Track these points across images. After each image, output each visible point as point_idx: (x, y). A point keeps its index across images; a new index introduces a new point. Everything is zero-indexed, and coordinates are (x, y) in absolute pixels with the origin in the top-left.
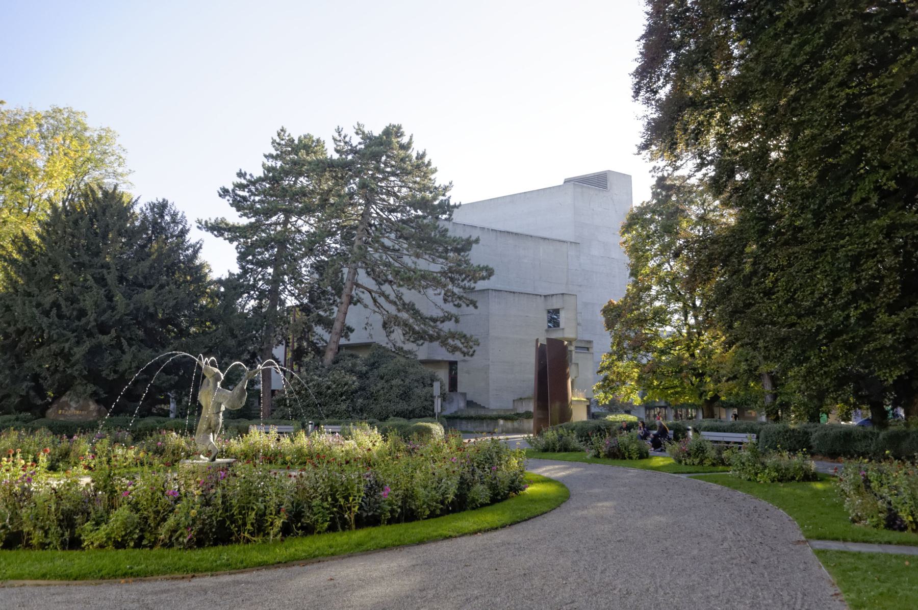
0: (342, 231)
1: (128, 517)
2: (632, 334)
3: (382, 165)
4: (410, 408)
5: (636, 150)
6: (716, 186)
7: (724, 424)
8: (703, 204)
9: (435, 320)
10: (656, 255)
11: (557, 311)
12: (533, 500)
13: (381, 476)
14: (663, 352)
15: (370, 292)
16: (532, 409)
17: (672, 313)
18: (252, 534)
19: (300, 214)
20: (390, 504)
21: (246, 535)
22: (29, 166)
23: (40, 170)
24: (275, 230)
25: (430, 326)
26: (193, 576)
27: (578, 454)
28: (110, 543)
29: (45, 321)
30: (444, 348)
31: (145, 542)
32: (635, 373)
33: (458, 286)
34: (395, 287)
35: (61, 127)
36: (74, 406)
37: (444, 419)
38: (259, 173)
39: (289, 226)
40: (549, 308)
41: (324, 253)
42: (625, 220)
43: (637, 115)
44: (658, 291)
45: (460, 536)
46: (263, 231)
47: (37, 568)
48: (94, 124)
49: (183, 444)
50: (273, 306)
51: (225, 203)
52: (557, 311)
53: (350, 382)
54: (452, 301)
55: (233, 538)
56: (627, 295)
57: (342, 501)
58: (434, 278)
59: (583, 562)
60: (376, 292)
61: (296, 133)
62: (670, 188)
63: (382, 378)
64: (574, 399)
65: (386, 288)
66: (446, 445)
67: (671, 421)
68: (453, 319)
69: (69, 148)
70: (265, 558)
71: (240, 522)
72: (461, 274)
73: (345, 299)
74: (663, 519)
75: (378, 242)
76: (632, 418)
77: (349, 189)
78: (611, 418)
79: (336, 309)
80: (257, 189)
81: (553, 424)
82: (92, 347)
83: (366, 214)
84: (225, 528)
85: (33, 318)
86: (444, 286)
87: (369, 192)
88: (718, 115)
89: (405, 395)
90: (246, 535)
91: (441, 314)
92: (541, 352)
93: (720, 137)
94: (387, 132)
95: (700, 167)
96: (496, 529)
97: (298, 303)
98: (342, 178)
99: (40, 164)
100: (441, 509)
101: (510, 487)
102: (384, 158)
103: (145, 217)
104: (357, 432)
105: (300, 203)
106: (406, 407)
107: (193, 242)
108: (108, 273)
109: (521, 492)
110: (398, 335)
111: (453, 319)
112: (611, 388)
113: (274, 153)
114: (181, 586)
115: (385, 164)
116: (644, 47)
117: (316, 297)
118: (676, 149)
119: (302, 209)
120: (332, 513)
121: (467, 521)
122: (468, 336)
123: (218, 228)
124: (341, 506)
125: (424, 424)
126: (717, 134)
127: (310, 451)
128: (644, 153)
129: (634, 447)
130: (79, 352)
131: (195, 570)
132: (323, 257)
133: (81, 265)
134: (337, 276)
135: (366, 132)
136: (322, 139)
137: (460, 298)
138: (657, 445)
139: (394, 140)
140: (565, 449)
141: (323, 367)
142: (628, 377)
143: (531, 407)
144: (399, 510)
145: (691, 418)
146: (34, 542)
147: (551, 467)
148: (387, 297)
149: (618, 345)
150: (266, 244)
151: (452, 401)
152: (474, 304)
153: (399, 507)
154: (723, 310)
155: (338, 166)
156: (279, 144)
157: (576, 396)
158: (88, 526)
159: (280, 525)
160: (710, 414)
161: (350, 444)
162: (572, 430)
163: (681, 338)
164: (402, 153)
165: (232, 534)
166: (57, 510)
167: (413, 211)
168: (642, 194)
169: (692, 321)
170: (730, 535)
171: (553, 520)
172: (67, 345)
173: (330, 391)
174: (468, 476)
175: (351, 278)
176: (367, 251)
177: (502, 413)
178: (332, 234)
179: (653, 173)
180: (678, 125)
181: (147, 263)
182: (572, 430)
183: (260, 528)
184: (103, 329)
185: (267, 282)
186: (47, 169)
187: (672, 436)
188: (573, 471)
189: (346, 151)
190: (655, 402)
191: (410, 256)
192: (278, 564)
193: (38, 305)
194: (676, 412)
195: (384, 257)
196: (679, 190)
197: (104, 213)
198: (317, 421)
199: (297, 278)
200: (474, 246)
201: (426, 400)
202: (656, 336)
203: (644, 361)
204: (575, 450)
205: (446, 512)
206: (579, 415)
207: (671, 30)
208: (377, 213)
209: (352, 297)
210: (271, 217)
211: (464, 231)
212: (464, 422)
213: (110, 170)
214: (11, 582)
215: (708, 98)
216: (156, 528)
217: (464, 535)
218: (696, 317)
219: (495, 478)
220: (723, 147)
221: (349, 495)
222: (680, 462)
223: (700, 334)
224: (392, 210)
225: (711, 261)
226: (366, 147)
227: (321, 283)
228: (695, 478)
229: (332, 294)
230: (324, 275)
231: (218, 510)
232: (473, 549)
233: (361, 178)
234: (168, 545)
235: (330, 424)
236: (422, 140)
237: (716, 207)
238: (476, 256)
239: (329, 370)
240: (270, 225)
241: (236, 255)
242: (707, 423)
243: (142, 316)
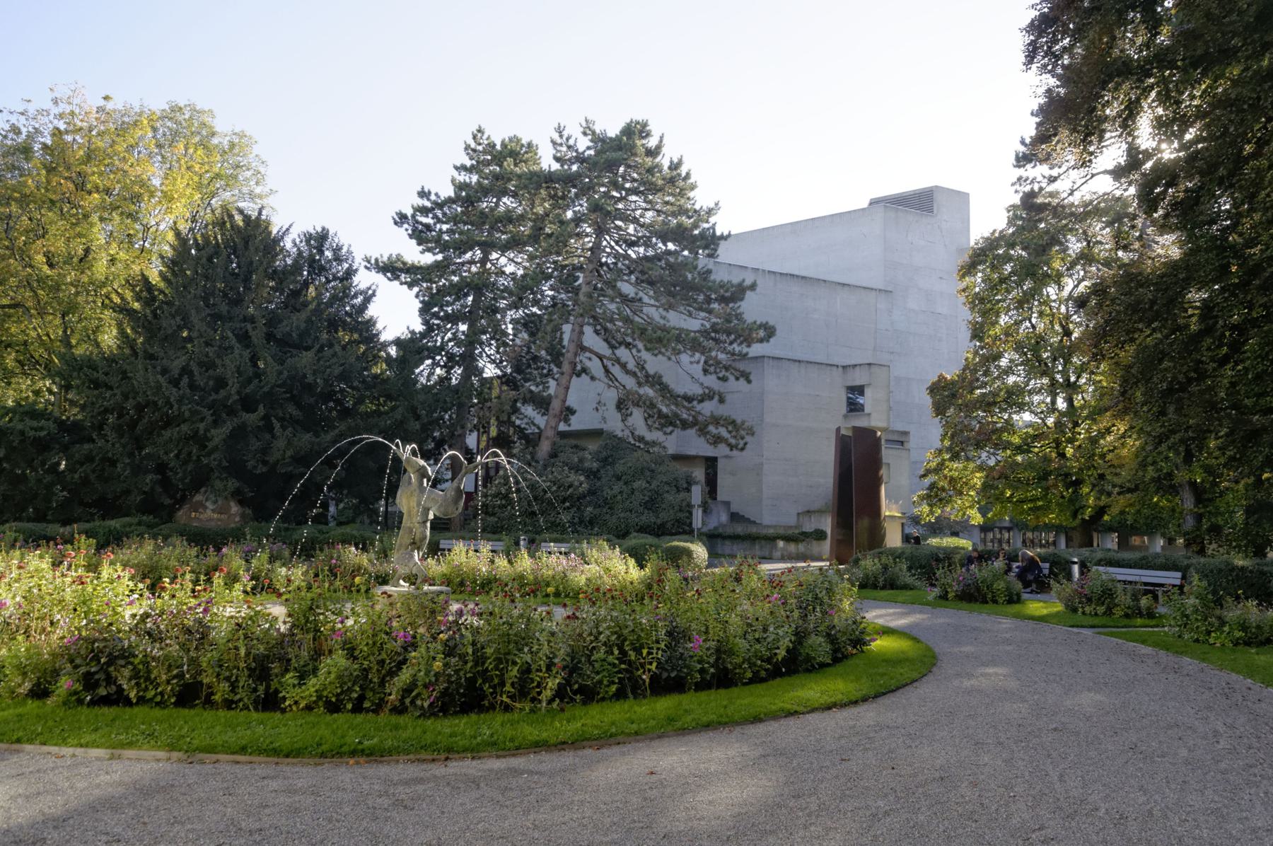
1: (346, 669)
4: (659, 522)
9: (689, 399)
11: (860, 390)
14: (1019, 449)
15: (601, 358)
18: (512, 697)
19: (504, 248)
20: (699, 662)
21: (505, 698)
22: (143, 184)
23: (156, 190)
24: (469, 271)
26: (447, 759)
28: (321, 703)
29: (174, 393)
30: (702, 439)
31: (367, 704)
32: (978, 479)
33: (724, 351)
34: (634, 351)
35: (182, 131)
36: (211, 507)
37: (705, 538)
38: (448, 191)
39: (489, 265)
41: (536, 303)
46: (454, 273)
47: (231, 737)
48: (224, 125)
49: (365, 562)
50: (466, 377)
51: (402, 233)
52: (860, 390)
53: (576, 483)
55: (486, 703)
57: (632, 655)
60: (609, 359)
61: (498, 136)
63: (619, 478)
65: (623, 353)
68: (717, 398)
69: (191, 158)
70: (545, 735)
71: (496, 681)
72: (729, 334)
73: (566, 367)
78: (934, 541)
79: (552, 383)
80: (444, 214)
82: (234, 428)
83: (596, 249)
84: (476, 690)
85: (159, 387)
87: (602, 216)
89: (652, 504)
90: (505, 698)
97: (499, 373)
98: (563, 197)
99: (156, 182)
102: (622, 169)
103: (300, 253)
105: (503, 233)
107: (362, 286)
108: (254, 329)
110: (637, 418)
111: (717, 398)
113: (468, 163)
114: (437, 773)
117: (522, 368)
119: (508, 242)
121: (812, 690)
122: (739, 421)
123: (392, 269)
125: (682, 544)
127: (536, 578)
130: (219, 435)
131: (449, 750)
132: (535, 310)
133: (217, 317)
135: (598, 131)
136: (534, 143)
139: (639, 143)
140: (892, 584)
143: (827, 524)
146: (217, 697)
147: (883, 611)
148: (623, 366)
150: (459, 291)
152: (746, 376)
156: (474, 150)
157: (889, 509)
158: (290, 678)
159: (555, 687)
165: (483, 697)
166: (248, 654)
167: (660, 245)
168: (989, 216)
172: (202, 426)
177: (781, 532)
179: (1017, 187)
181: (303, 315)
183: (525, 690)
184: (248, 404)
185: (459, 343)
186: (164, 188)
189: (570, 160)
192: (562, 745)
193: (165, 371)
197: (246, 248)
198: (531, 535)
199: (498, 335)
202: (1009, 424)
203: (992, 462)
204: (906, 587)
206: (893, 539)
208: (612, 248)
210: (465, 253)
212: (727, 542)
213: (245, 190)
214: (201, 756)
216: (382, 683)
217: (813, 710)
221: (642, 647)
222: (1075, 610)
224: (632, 244)
226: (598, 153)
228: (1112, 635)
229: (546, 361)
231: (466, 663)
232: (822, 727)
234: (399, 710)
236: (676, 142)
238: (752, 309)
240: (463, 264)
241: (417, 305)
243: (297, 388)
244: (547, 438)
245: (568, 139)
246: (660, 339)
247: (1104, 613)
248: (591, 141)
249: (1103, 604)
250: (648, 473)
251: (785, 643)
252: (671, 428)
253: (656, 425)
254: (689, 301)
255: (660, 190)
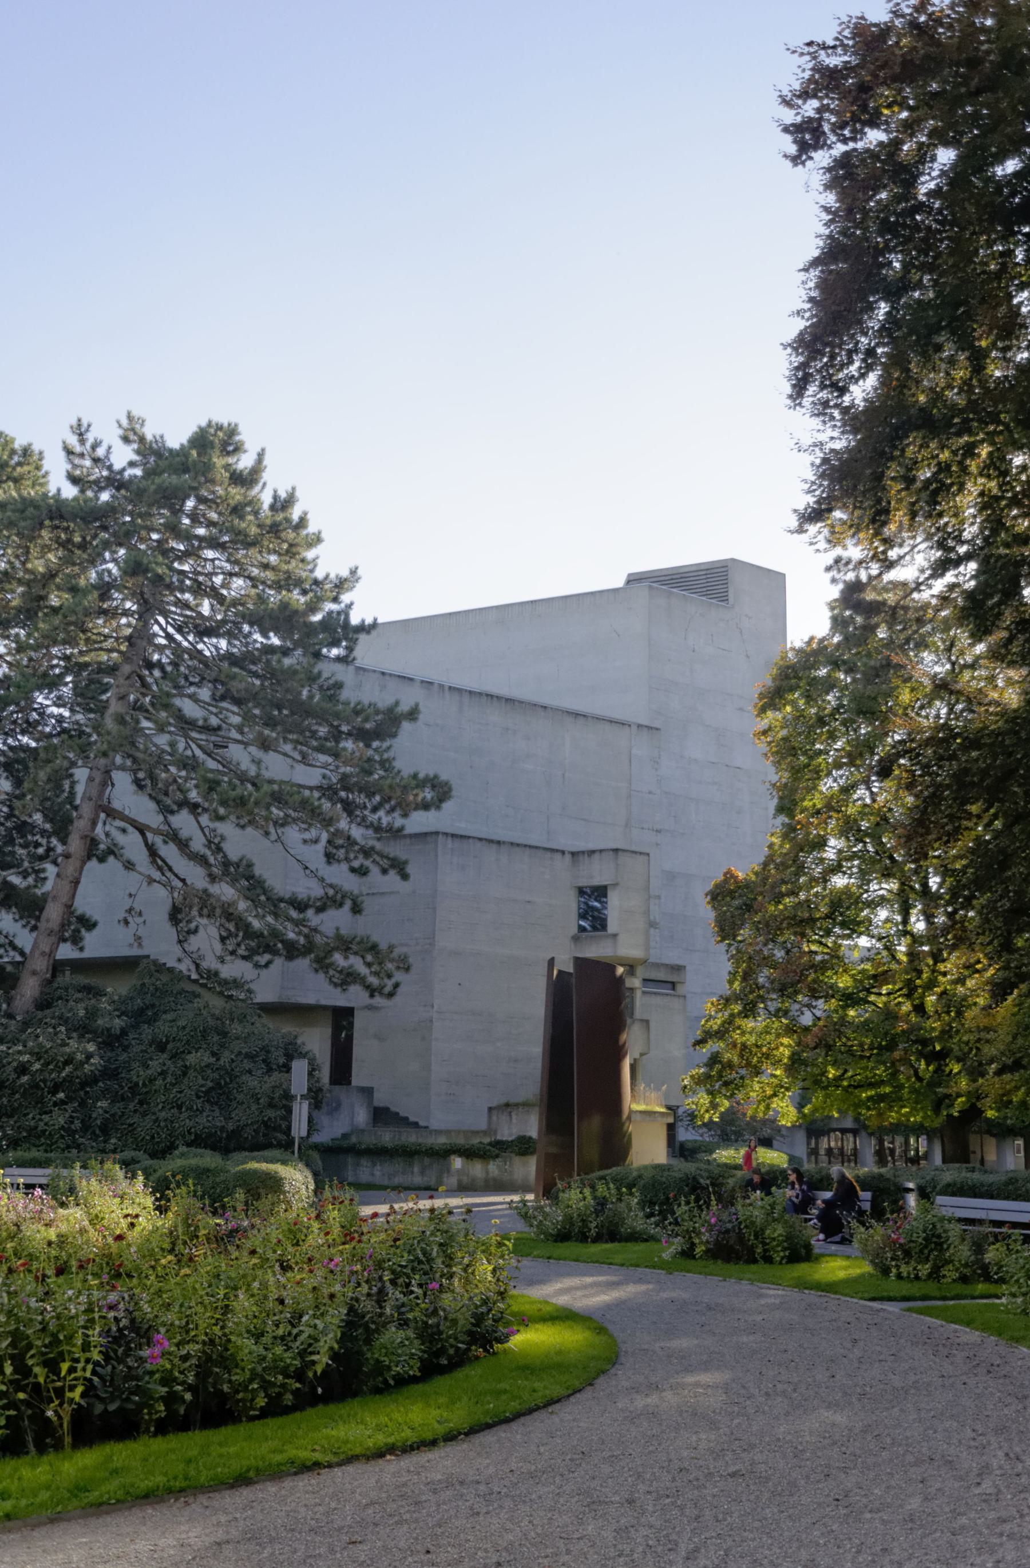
0: (77, 675)
2: (779, 954)
3: (186, 521)
4: (231, 1126)
5: (794, 522)
6: (977, 612)
7: (990, 1178)
8: (949, 649)
9: (301, 906)
10: (838, 766)
11: (601, 892)
12: (531, 1367)
13: (146, 1308)
14: (850, 999)
15: (142, 830)
16: (533, 1132)
17: (874, 904)
25: (289, 919)
27: (641, 1247)
30: (321, 975)
33: (363, 822)
34: (204, 819)
37: (315, 1156)
40: (583, 882)
42: (767, 679)
43: (792, 444)
44: (840, 852)
45: (340, 1464)
52: (601, 892)
53: (79, 1057)
54: (347, 859)
56: (769, 860)
58: (304, 803)
59: (644, 1531)
60: (157, 832)
62: (873, 609)
63: (162, 1048)
64: (636, 1107)
65: (183, 821)
66: (316, 1225)
67: (869, 1167)
72: (370, 795)
73: (76, 844)
74: (839, 1418)
75: (167, 706)
76: (771, 1157)
77: (100, 575)
79: (51, 870)
81: (586, 1169)
83: (140, 638)
86: (328, 822)
87: (150, 585)
88: (984, 451)
89: (220, 1094)
91: (316, 891)
92: (560, 990)
93: (987, 502)
94: (202, 440)
95: (940, 568)
96: (433, 1443)
98: (83, 546)
100: (296, 1393)
101: (470, 1333)
102: (190, 504)
104: (89, 1185)
106: (220, 1122)
109: (497, 1347)
110: (207, 939)
111: (348, 904)
112: (726, 1084)
115: (194, 517)
116: (817, 286)
118: (885, 523)
120: (13, 1405)
121: (361, 1424)
122: (383, 946)
124: (37, 1386)
125: (264, 1166)
126: (982, 494)
128: (813, 529)
129: (778, 1231)
132: (25, 740)
134: (59, 787)
135: (149, 437)
136: (36, 448)
137: (367, 852)
138: (832, 1227)
139: (218, 461)
140: (612, 1233)
141: (10, 1016)
142: (767, 1056)
143: (531, 1126)
144: (188, 1396)
145: (915, 1160)
147: (575, 1281)
148: (183, 845)
149: (746, 977)
151: (338, 1107)
152: (400, 868)
153: (189, 1388)
154: (991, 906)
155: (74, 517)
157: (641, 1101)
160: (959, 1153)
161: (72, 1217)
162: (630, 1187)
163: (894, 966)
164: (236, 493)
167: (257, 636)
168: (809, 618)
169: (920, 926)
170: (998, 1460)
171: (575, 1418)
173: (25, 1079)
174: (367, 1306)
175: (94, 793)
176: (139, 730)
177: (460, 1141)
178: (51, 683)
180: (893, 470)
182: (630, 1187)
187: (867, 1206)
188: (629, 1291)
189: (96, 482)
190: (831, 1117)
191: (246, 744)
194: (881, 1142)
195: (181, 745)
196: (893, 614)
200: (406, 725)
201: (271, 1105)
204: (635, 1237)
205: (307, 1400)
206: (649, 1149)
207: (882, 252)
208: (169, 637)
209: (94, 842)
211: (383, 687)
215: (962, 411)
218: (929, 917)
219: (435, 1312)
220: (995, 524)
222: (886, 1271)
223: (937, 957)
224: (206, 630)
225: (964, 785)
226: (148, 474)
227: (17, 803)
228: (920, 1312)
229: (43, 833)
230: (26, 785)
233: (131, 548)
235: (22, 1164)
236: (290, 462)
237: (978, 658)
238: (411, 752)
239: (26, 1024)
242: (951, 1174)
244: (34, 973)
245: (95, 446)
246: (247, 801)
247: (930, 1276)
248: (138, 452)
249: (927, 1260)
250: (216, 1038)
251: (329, 1341)
252: (267, 957)
253: (242, 951)
254: (304, 738)
255: (253, 544)
